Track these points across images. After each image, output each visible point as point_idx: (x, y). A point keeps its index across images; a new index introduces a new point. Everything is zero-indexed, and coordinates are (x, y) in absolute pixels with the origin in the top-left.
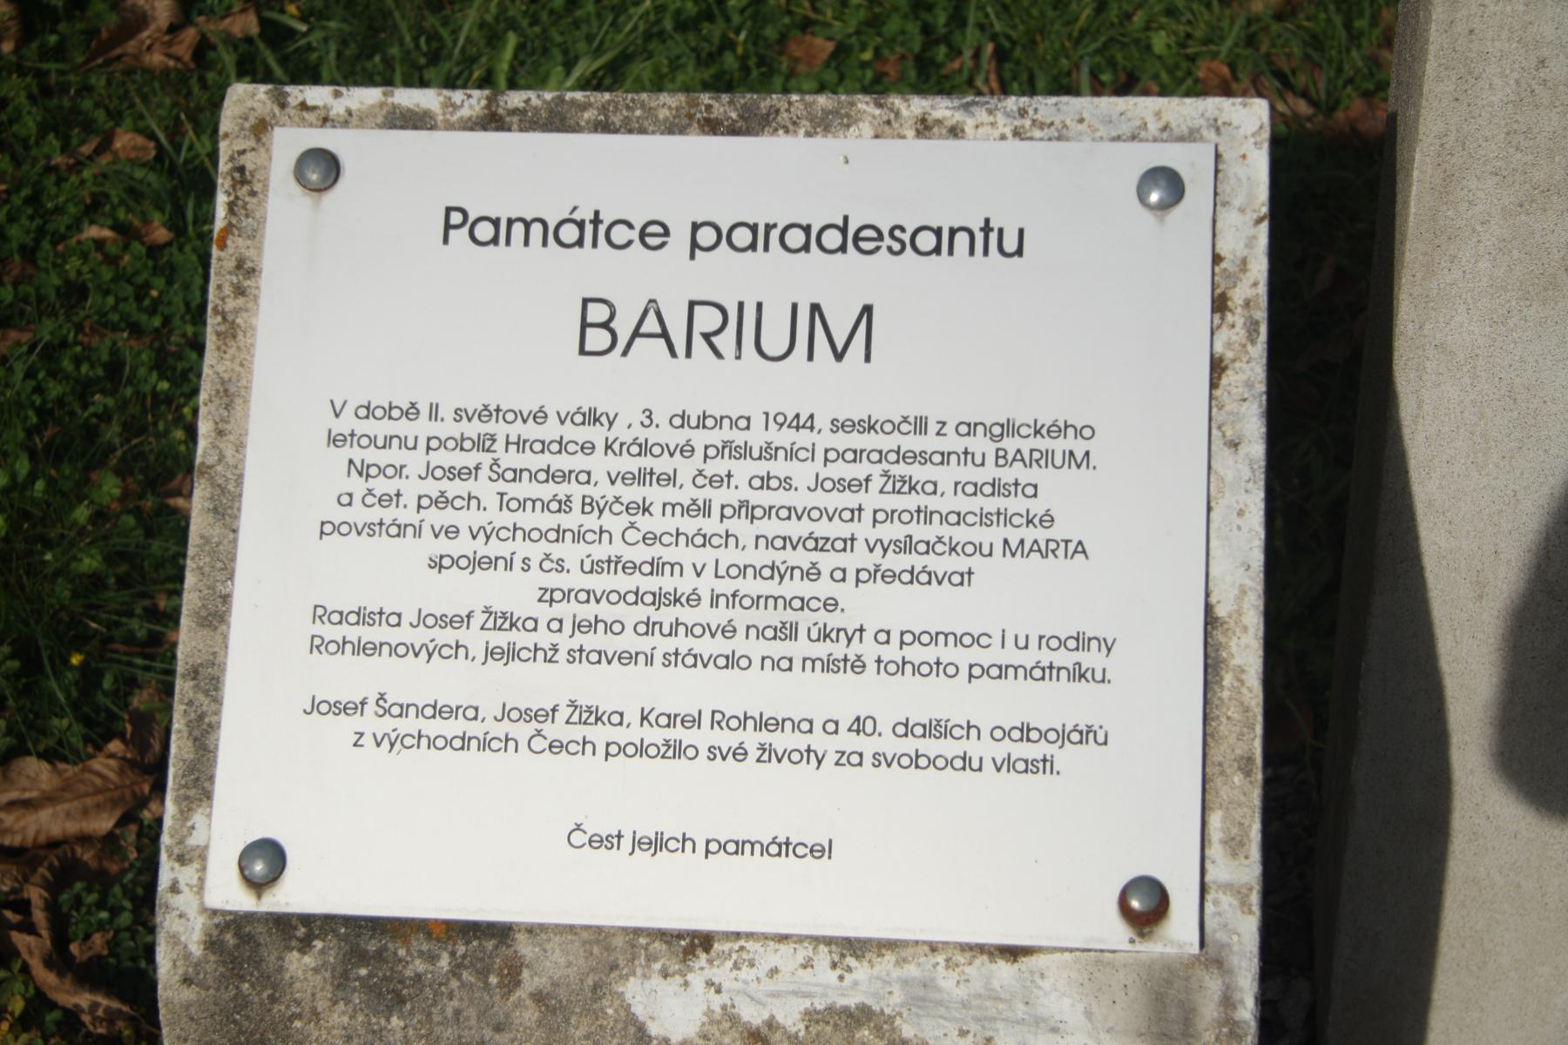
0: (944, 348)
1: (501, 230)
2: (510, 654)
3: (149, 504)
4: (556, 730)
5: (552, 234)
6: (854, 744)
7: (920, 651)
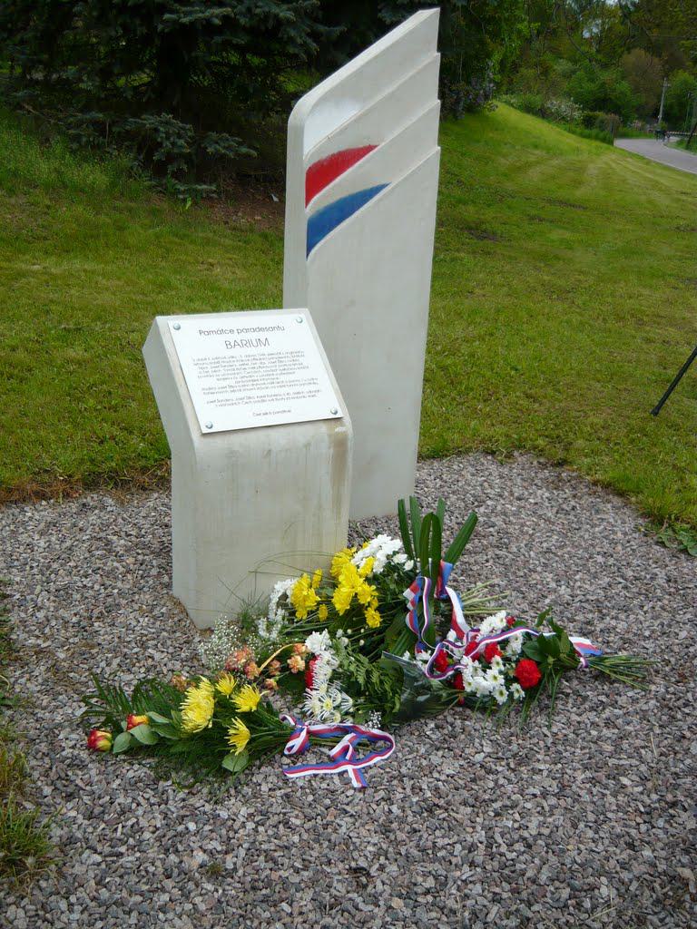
0: (278, 343)
1: (209, 333)
2: (234, 391)
3: (42, 433)
4: (245, 400)
5: (216, 332)
6: (288, 397)
7: (292, 383)
